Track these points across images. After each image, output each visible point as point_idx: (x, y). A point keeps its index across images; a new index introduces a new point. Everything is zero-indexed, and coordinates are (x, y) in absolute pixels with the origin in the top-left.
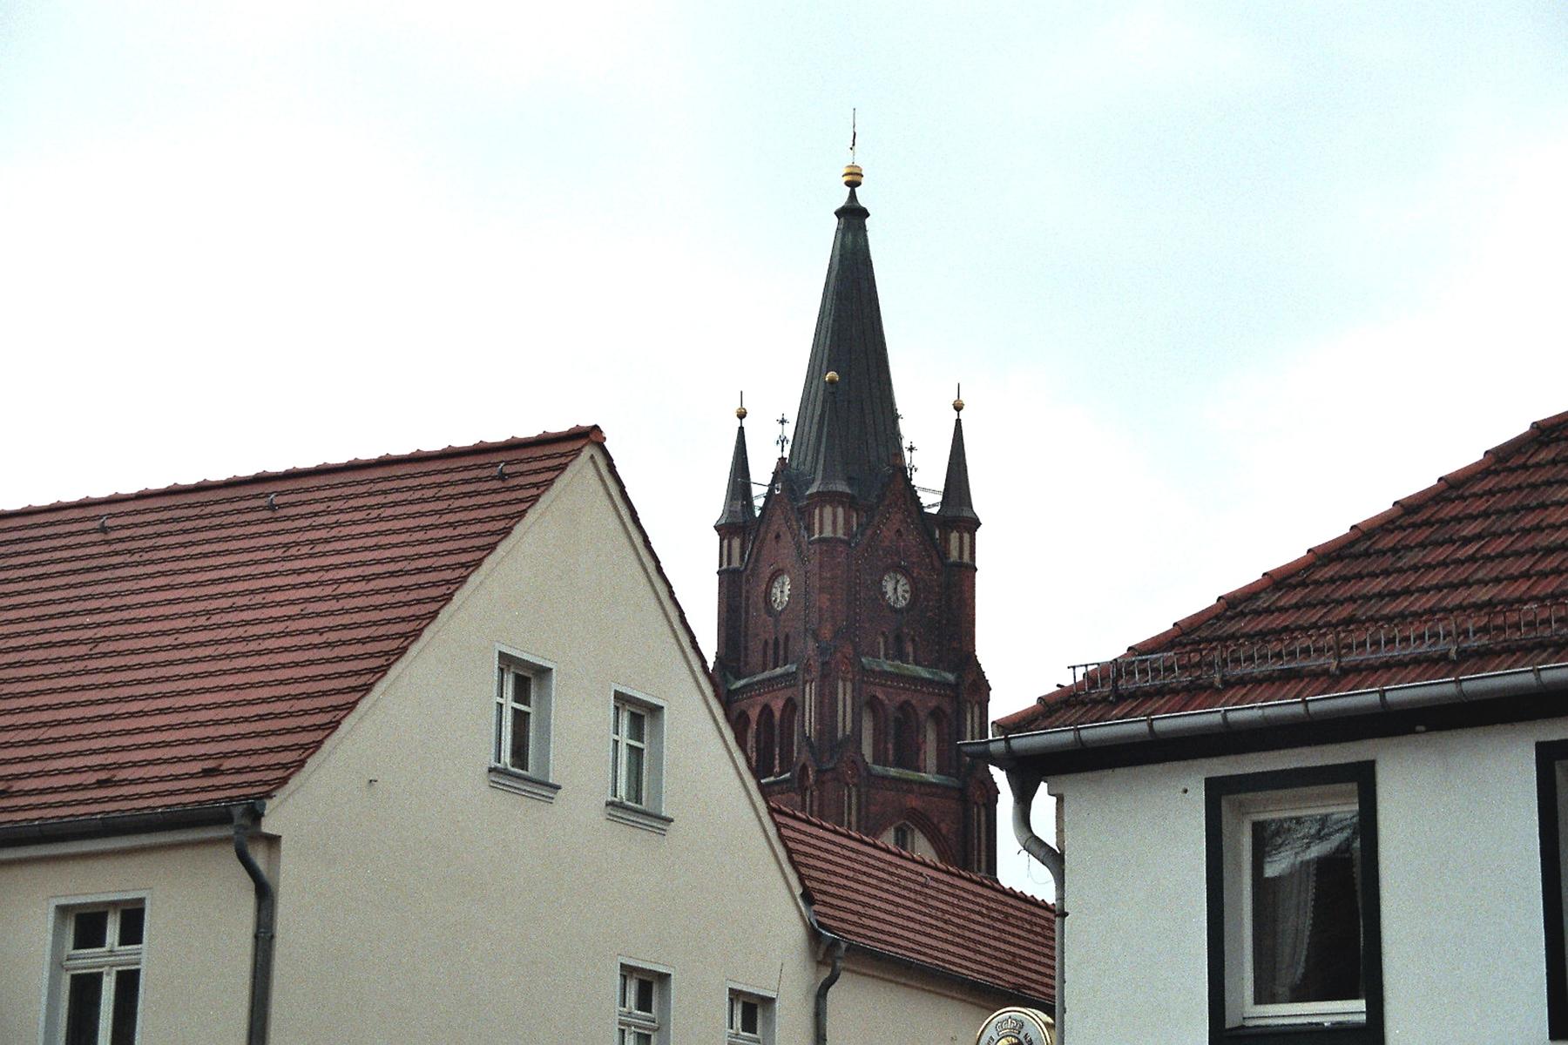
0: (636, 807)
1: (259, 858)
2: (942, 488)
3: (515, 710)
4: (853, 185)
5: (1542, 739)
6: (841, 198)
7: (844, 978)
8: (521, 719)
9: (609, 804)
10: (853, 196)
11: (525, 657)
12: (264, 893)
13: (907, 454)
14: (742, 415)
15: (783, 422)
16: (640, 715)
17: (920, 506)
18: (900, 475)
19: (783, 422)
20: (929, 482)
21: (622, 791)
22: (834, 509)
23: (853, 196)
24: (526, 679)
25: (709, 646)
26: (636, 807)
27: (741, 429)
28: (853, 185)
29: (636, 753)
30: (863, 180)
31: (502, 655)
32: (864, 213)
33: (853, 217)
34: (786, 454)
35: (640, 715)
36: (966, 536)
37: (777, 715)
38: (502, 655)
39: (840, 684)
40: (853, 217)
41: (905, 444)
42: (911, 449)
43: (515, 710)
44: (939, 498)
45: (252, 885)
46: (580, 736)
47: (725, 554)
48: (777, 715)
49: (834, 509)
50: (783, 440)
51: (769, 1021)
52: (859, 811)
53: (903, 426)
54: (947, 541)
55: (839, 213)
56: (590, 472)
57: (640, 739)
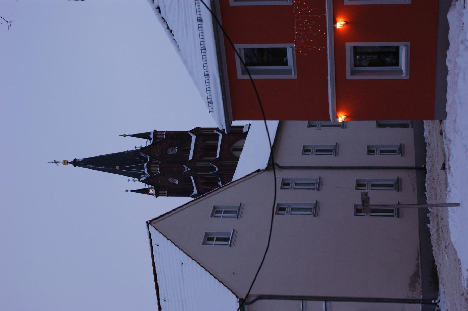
0: (237, 212)
1: (251, 299)
2: (146, 140)
3: (216, 241)
4: (68, 163)
5: (398, 67)
6: (71, 166)
7: (277, 162)
8: (218, 239)
9: (237, 218)
10: (70, 163)
11: (203, 238)
12: (261, 297)
13: (137, 149)
14: (127, 191)
15: (129, 180)
16: (216, 211)
17: (151, 145)
18: (143, 150)
19: (129, 180)
20: (143, 143)
21: (234, 215)
22: (151, 167)
23: (70, 163)
24: (208, 239)
25: (187, 199)
26: (237, 212)
27: (131, 191)
28: (68, 163)
29: (225, 212)
30: (67, 160)
31: (203, 244)
32: (75, 160)
33: (76, 163)
34: (138, 179)
35: (216, 211)
36: (158, 133)
37: (205, 181)
38: (203, 244)
39: (197, 165)
40: (76, 163)
41: (135, 149)
42: (136, 147)
43: (216, 241)
44: (149, 140)
45: (259, 301)
46: (222, 226)
47: (164, 195)
48: (205, 181)
49: (151, 167)
50: (134, 180)
51: (287, 180)
52: (228, 160)
53: (130, 149)
54: (160, 138)
55: (75, 166)
56: (156, 224)
57: (222, 211)
